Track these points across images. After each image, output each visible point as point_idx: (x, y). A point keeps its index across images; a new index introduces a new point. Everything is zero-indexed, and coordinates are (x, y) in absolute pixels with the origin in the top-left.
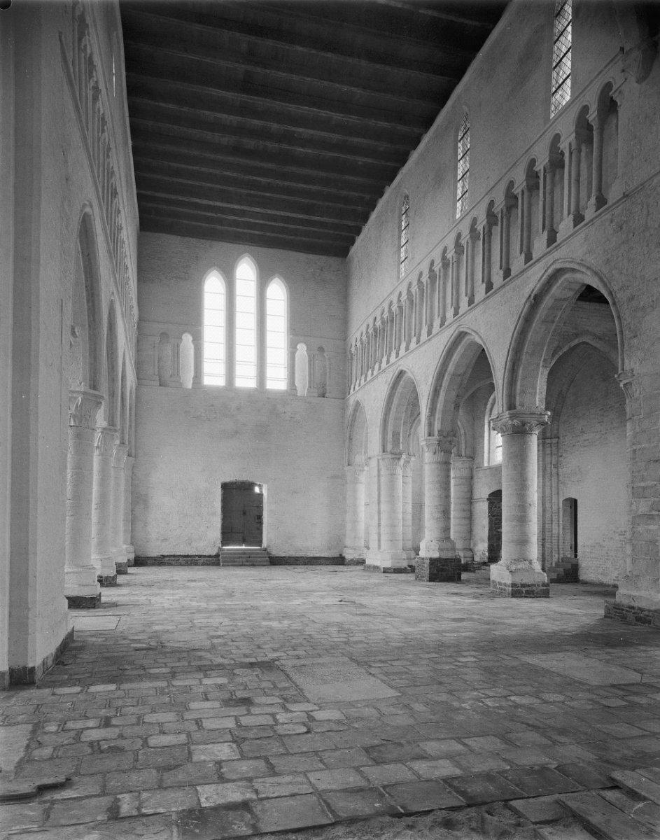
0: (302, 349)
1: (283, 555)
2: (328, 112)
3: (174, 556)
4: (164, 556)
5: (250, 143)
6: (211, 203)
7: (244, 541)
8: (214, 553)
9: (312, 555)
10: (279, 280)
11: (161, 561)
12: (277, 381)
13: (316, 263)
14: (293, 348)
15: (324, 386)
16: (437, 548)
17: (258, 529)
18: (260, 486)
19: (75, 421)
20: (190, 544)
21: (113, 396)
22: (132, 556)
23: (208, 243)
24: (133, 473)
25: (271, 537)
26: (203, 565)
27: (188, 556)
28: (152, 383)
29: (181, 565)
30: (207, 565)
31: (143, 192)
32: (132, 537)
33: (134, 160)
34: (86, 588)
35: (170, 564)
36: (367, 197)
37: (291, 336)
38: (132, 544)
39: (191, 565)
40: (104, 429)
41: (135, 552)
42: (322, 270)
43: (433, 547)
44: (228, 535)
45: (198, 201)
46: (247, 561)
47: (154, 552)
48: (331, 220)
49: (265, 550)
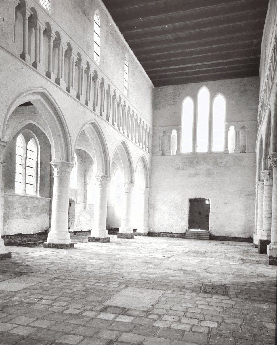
0: (232, 128)
1: (218, 235)
2: (208, 7)
3: (165, 233)
4: (161, 233)
5: (182, 34)
6: (177, 67)
7: (199, 227)
8: (184, 233)
9: (234, 236)
10: (220, 94)
11: (159, 235)
12: (218, 147)
13: (241, 82)
14: (227, 129)
15: (245, 147)
16: (266, 235)
17: (207, 222)
18: (209, 200)
19: (59, 174)
20: (173, 228)
21: (107, 162)
22: (147, 232)
23: (184, 85)
24: (149, 195)
25: (214, 225)
26: (178, 237)
27: (171, 233)
28: (158, 154)
29: (168, 237)
30: (180, 238)
31: (150, 70)
32: (148, 224)
33: (262, 38)
34: (60, 240)
35: (163, 236)
36: (255, 41)
37: (226, 123)
38: (148, 226)
39: (172, 237)
40: (102, 176)
41: (149, 230)
42: (244, 85)
43: (264, 234)
44: (192, 224)
45: (172, 67)
46: (197, 237)
47: (157, 231)
48: (235, 59)
49: (209, 232)
